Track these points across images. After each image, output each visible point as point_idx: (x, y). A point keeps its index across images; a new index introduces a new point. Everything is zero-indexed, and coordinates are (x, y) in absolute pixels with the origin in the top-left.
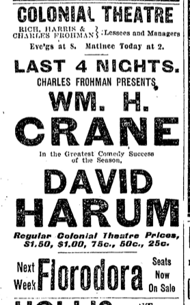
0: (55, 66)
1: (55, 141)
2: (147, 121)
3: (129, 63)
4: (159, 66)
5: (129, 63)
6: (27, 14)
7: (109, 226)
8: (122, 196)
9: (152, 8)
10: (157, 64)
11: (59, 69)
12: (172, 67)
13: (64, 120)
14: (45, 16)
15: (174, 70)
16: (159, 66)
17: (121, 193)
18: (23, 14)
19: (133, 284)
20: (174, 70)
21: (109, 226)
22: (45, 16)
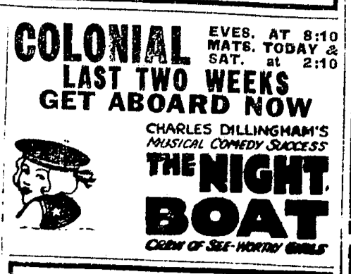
0: (280, 35)
1: (158, 36)
2: (237, 94)
3: (55, 95)
4: (240, 47)
5: (55, 95)
6: (35, 42)
7: (31, 191)
8: (261, 96)
9: (240, 43)
10: (239, 45)
11: (284, 38)
12: (249, 47)
13: (308, 40)
14: (78, 47)
15: (251, 50)
16: (240, 47)
17: (148, 199)
18: (27, 42)
19: (331, 37)
20: (251, 50)
21: (31, 191)
22: (78, 47)
